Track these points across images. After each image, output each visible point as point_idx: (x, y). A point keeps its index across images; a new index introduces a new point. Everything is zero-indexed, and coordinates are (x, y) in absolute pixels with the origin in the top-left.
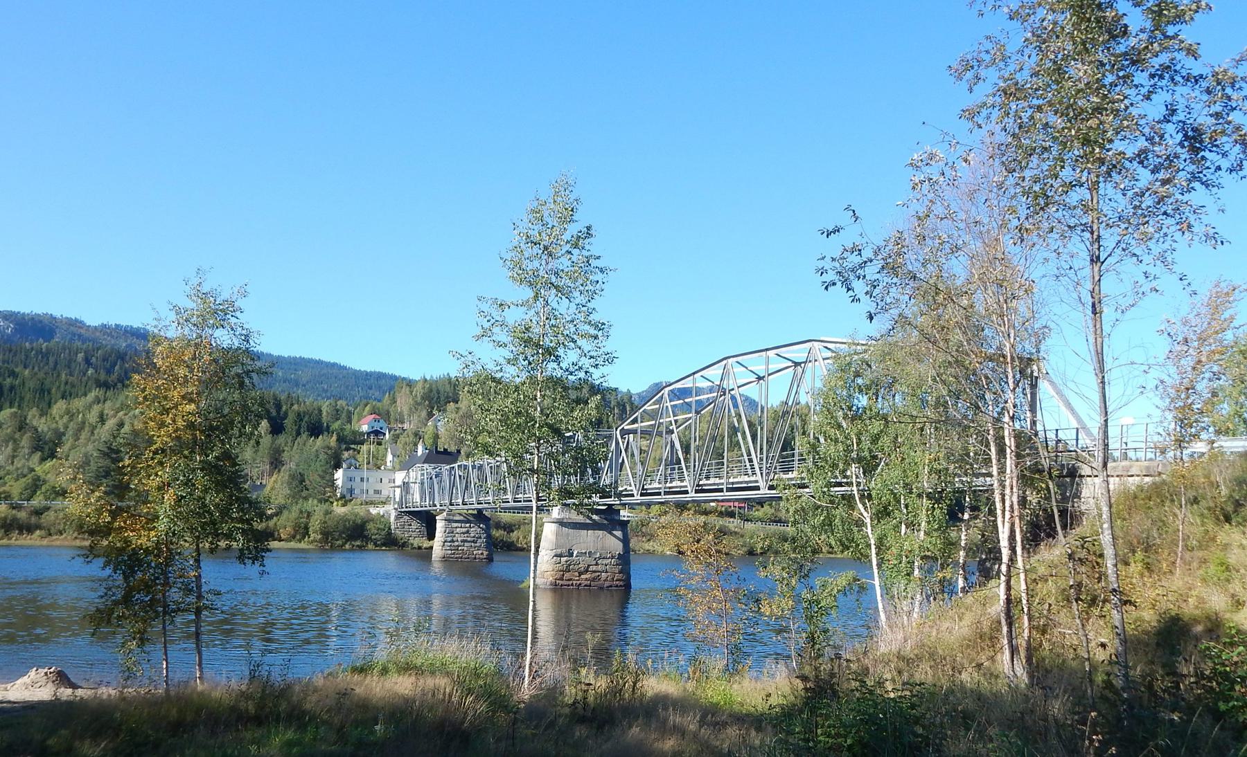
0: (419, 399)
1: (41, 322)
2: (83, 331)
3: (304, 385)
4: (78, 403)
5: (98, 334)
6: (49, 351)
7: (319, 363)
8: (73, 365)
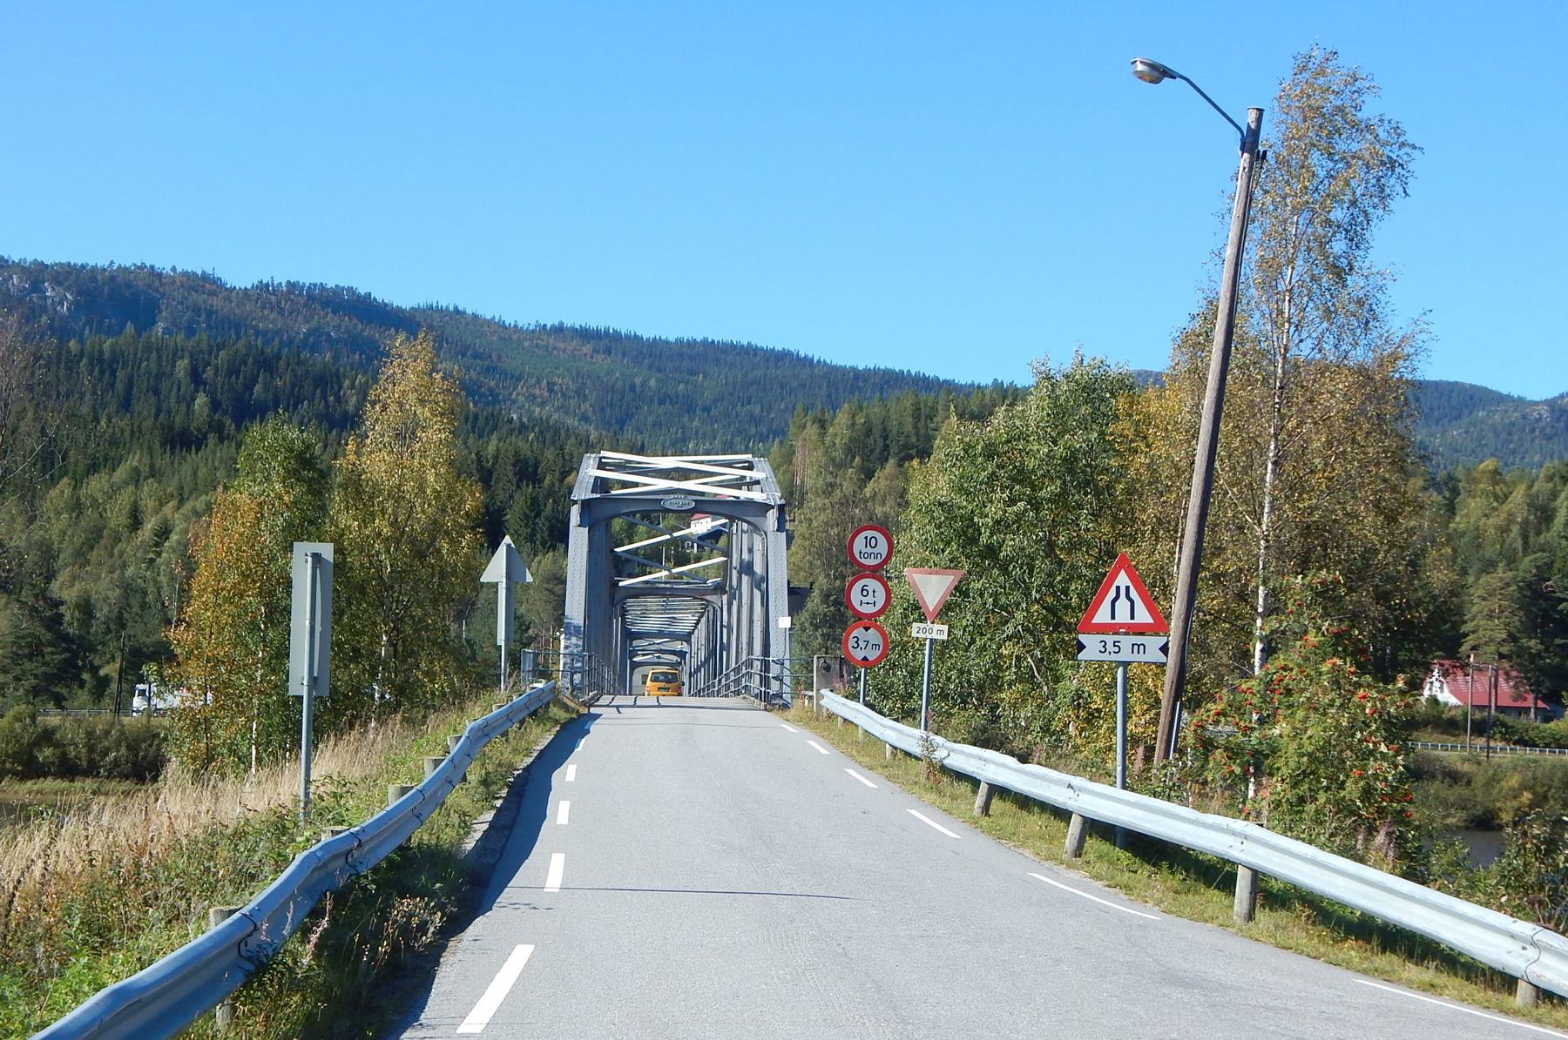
0: (839, 454)
1: (129, 285)
2: (216, 302)
3: (707, 409)
4: (96, 485)
5: (249, 307)
6: (117, 358)
7: (748, 353)
8: (164, 386)
